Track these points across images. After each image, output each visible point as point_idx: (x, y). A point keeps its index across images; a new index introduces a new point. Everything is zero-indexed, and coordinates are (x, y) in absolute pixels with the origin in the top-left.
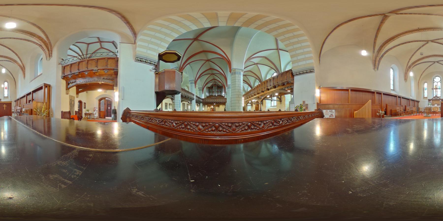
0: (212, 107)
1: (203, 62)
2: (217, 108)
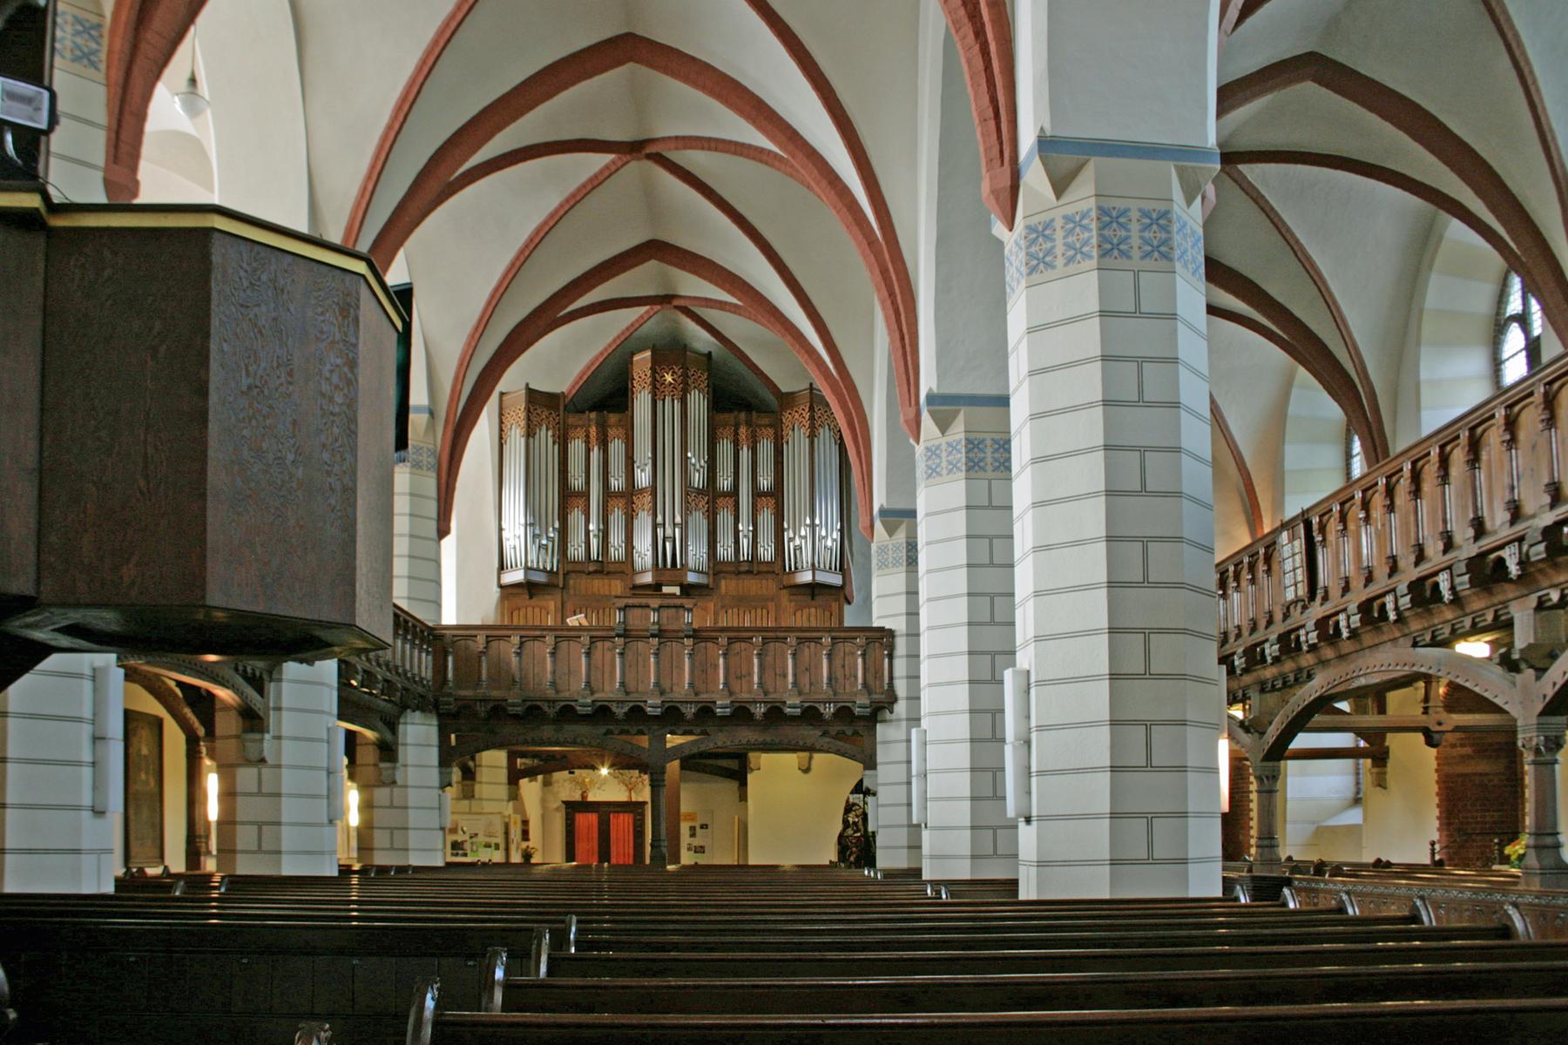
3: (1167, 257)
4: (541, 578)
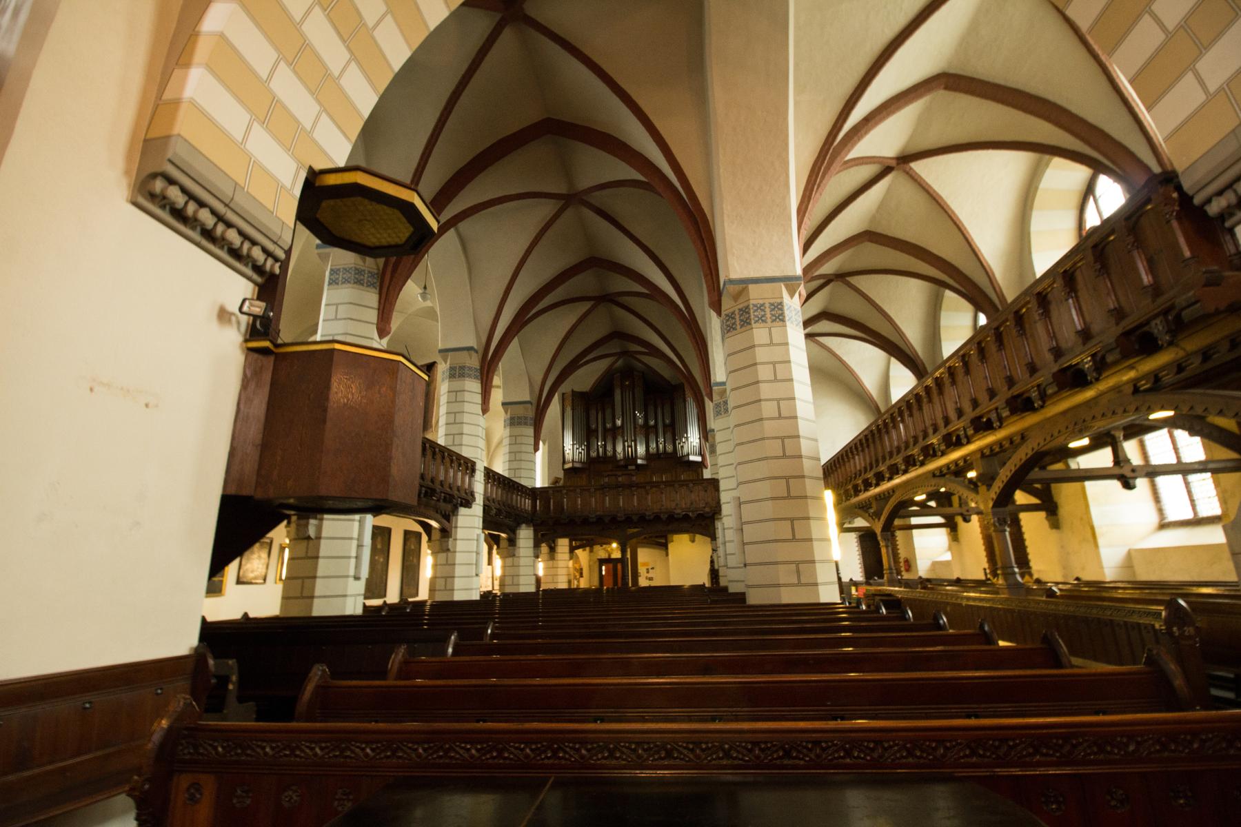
0: (614, 550)
1: (545, 210)
2: (645, 556)
3: (783, 320)
4: (577, 465)
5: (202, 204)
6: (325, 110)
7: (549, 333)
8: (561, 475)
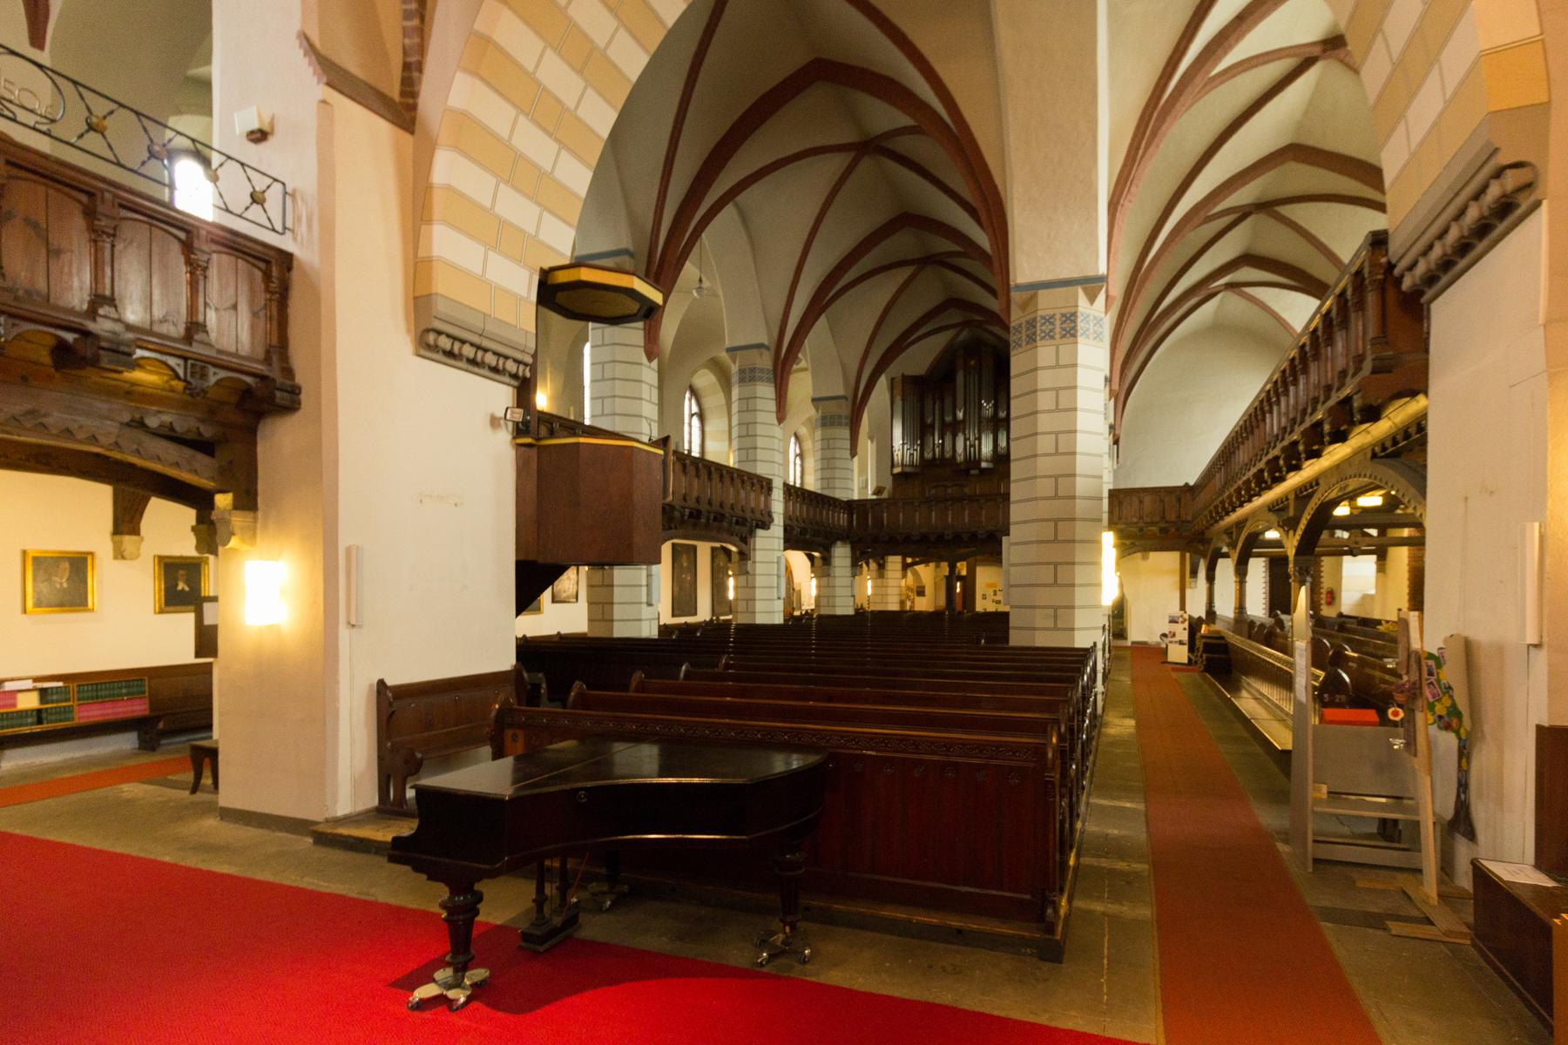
1: (833, 165)
3: (1074, 336)
4: (908, 470)
5: (463, 342)
6: (546, 209)
7: (863, 309)
8: (888, 484)
